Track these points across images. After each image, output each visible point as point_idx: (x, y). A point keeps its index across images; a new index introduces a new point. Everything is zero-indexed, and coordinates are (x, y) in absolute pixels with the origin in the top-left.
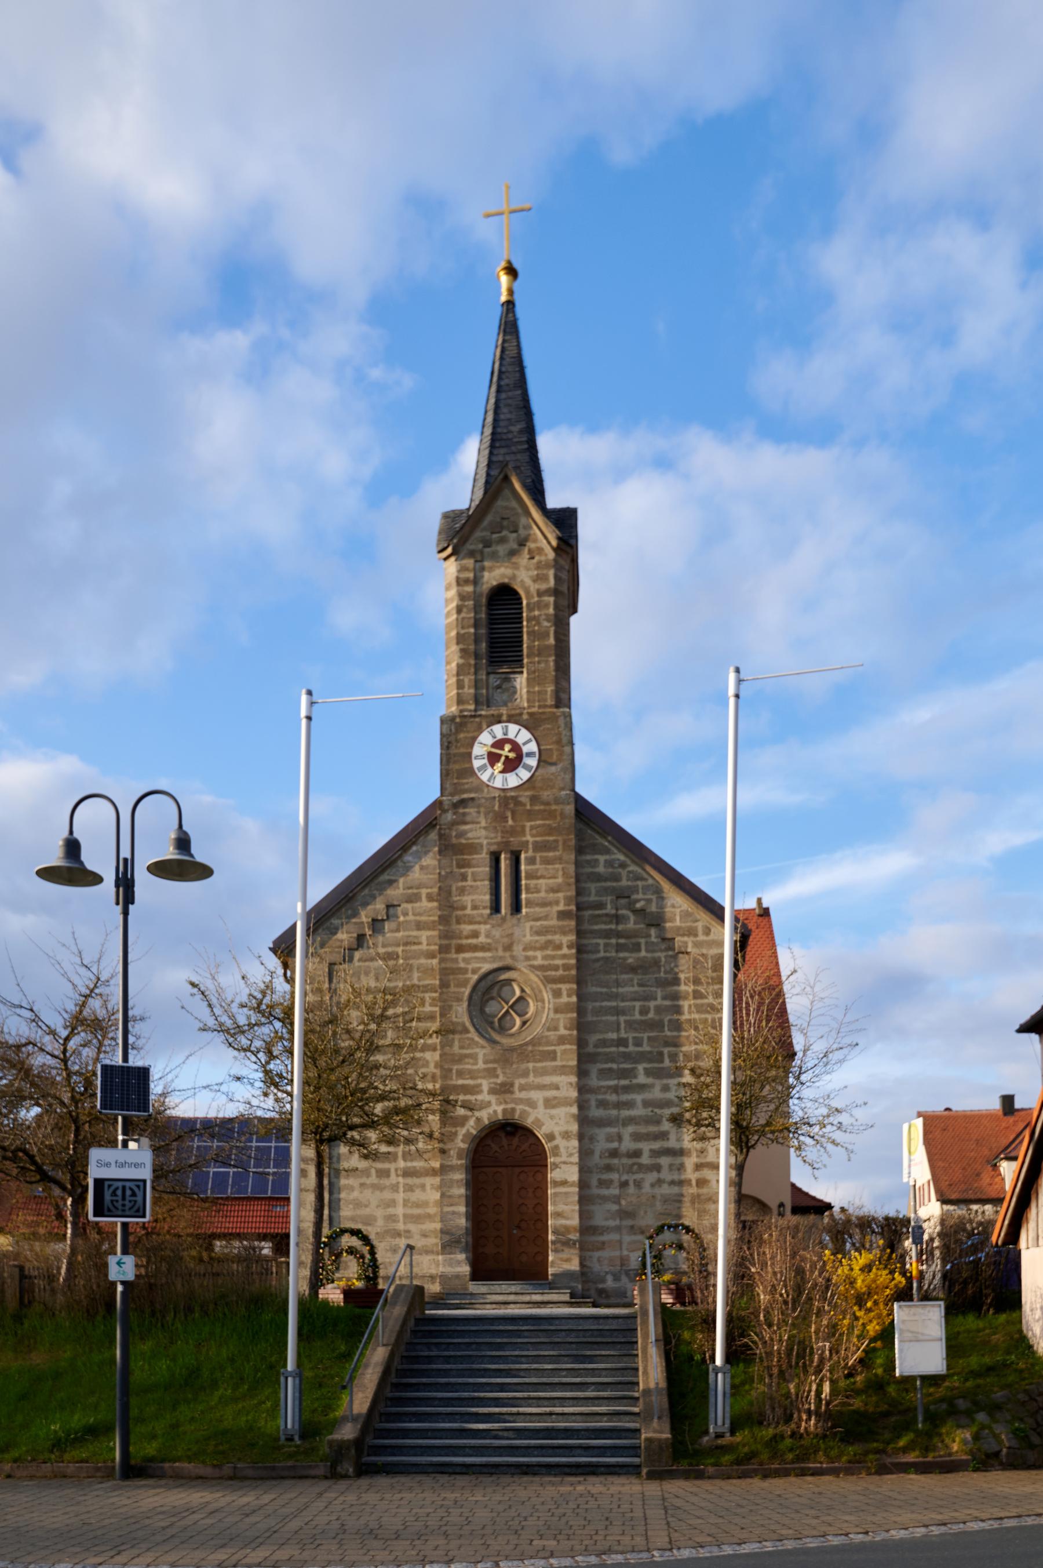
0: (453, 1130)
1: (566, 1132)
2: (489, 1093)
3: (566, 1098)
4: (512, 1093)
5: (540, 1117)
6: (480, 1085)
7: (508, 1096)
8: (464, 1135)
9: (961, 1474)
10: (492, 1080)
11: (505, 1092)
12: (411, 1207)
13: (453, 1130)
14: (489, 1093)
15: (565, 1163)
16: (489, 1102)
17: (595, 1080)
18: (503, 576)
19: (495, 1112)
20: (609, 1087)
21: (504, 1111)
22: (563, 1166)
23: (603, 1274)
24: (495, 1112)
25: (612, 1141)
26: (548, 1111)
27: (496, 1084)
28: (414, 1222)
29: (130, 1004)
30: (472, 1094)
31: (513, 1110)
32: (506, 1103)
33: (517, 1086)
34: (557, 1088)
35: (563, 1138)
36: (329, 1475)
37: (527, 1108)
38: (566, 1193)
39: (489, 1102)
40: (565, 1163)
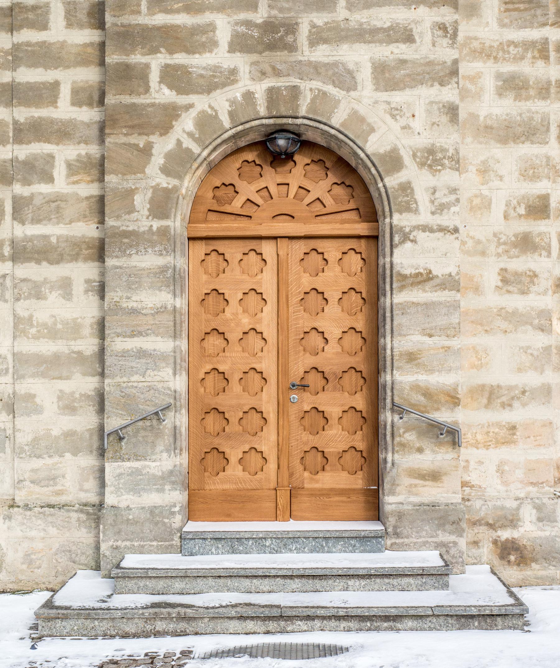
0: (141, 142)
1: (431, 151)
2: (232, 49)
3: (430, 63)
4: (292, 48)
5: (362, 110)
6: (211, 27)
7: (281, 55)
8: (169, 156)
9: (33, 31)
10: (243, 16)
11: (272, 47)
12: (36, 338)
13: (141, 142)
14: (232, 49)
15: (425, 228)
16: (234, 72)
17: (494, 25)
18: (305, 97)
19: (249, 96)
20: (529, 45)
21: (272, 93)
22: (421, 236)
23: (511, 504)
24: (249, 96)
25: (535, 178)
26: (384, 96)
27: (248, 23)
28: (43, 375)
29: (253, 205)
30: (190, 51)
31: (295, 92)
32: (277, 73)
33: (304, 30)
34: (409, 38)
35: (422, 165)
36: (94, 567)
37: (330, 89)
38: (428, 306)
39: (234, 72)
40: (425, 228)
